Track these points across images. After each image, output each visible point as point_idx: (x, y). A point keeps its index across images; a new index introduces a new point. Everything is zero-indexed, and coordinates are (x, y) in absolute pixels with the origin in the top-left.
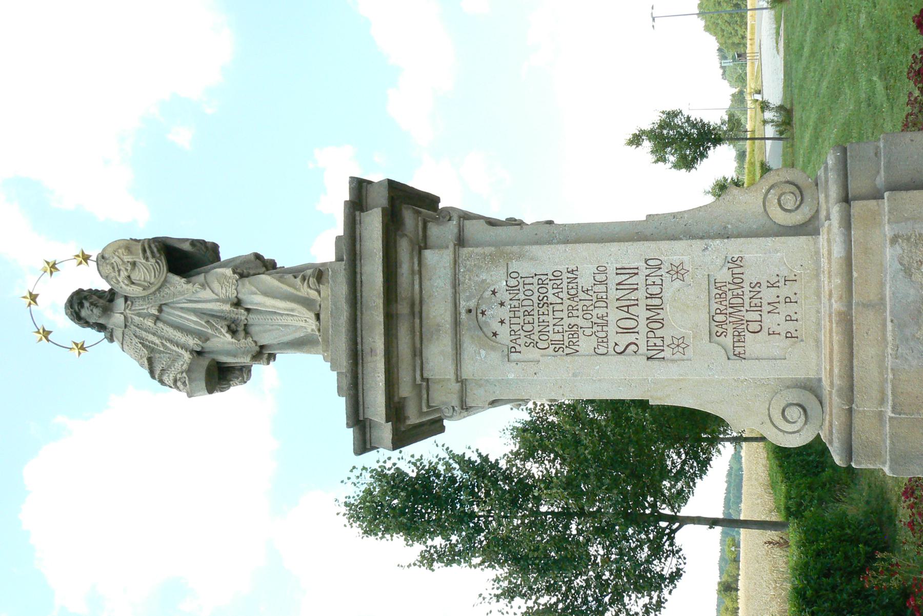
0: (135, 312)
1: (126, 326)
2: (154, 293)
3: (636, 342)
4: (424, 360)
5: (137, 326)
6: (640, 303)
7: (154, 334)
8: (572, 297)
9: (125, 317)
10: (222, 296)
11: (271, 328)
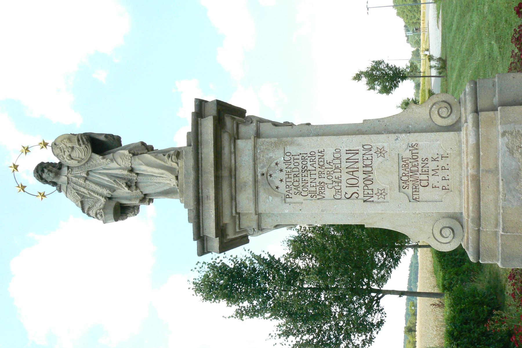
2: (84, 164)
4: (237, 203)
6: (359, 170)
7: (84, 188)
8: (321, 167)
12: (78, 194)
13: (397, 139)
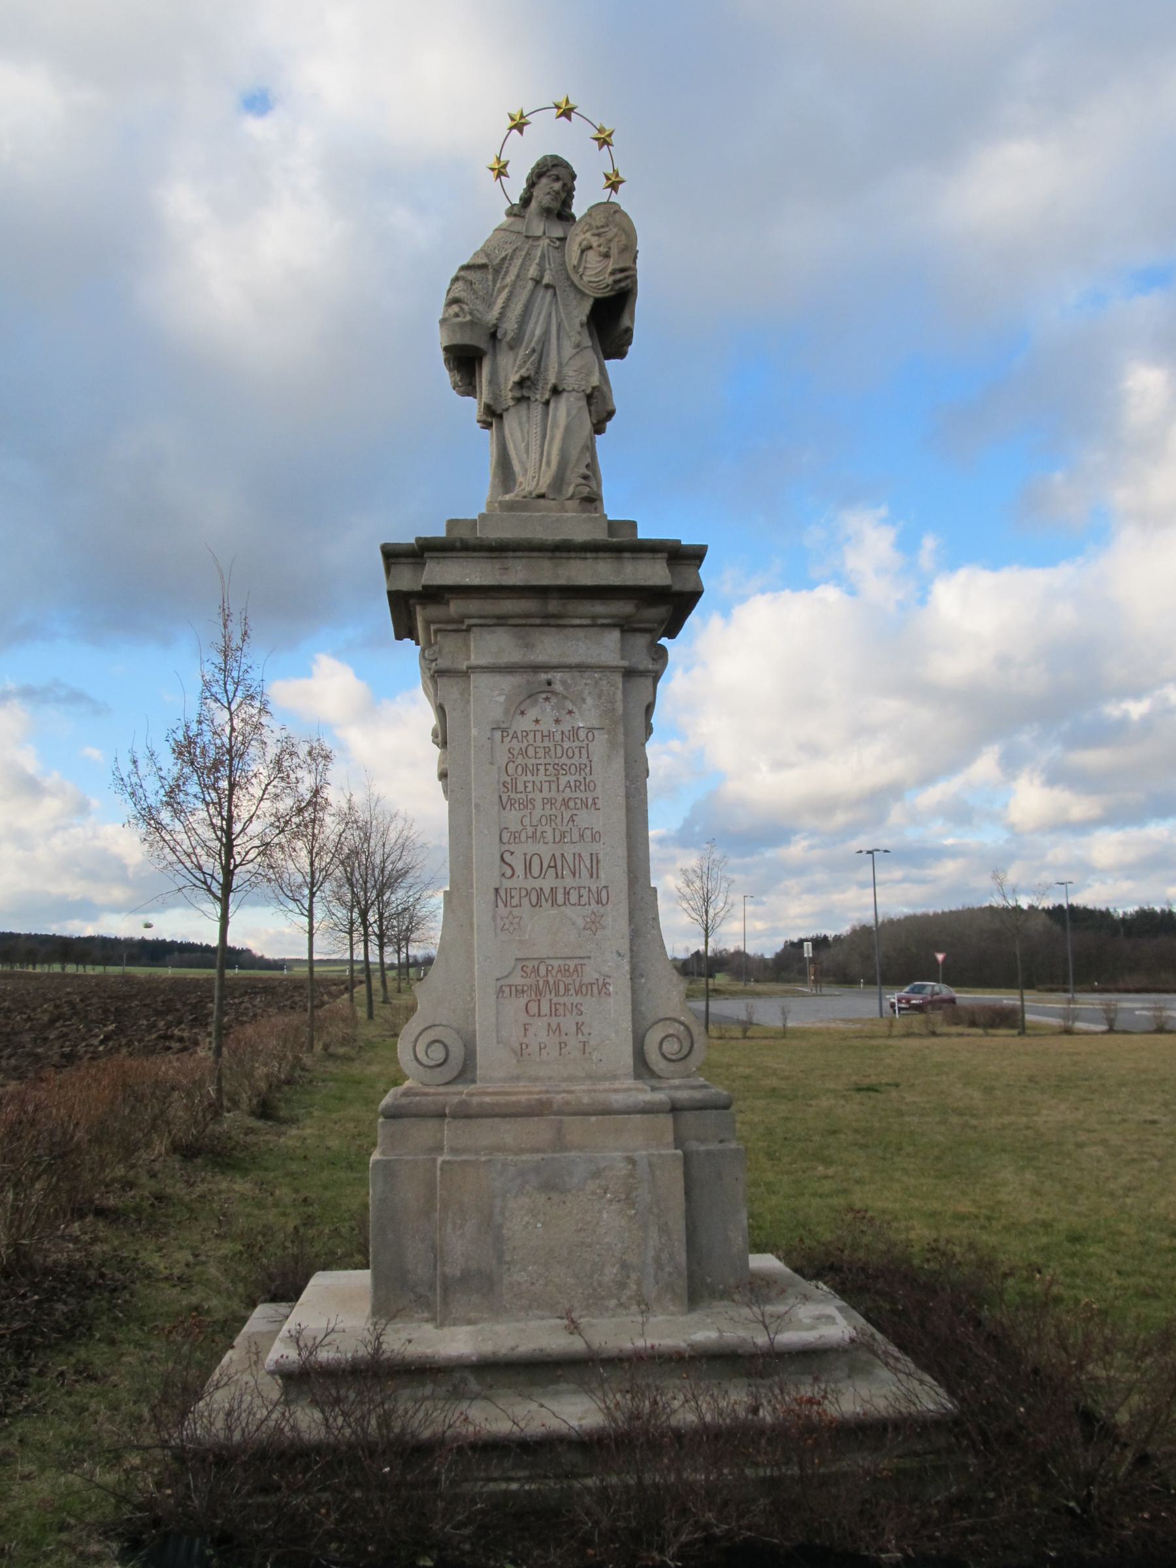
0: (546, 252)
1: (527, 237)
2: (568, 278)
3: (516, 875)
4: (492, 628)
5: (528, 254)
6: (559, 880)
7: (518, 276)
8: (565, 803)
9: (538, 238)
10: (566, 370)
11: (525, 430)
12: (504, 259)
13: (620, 955)
